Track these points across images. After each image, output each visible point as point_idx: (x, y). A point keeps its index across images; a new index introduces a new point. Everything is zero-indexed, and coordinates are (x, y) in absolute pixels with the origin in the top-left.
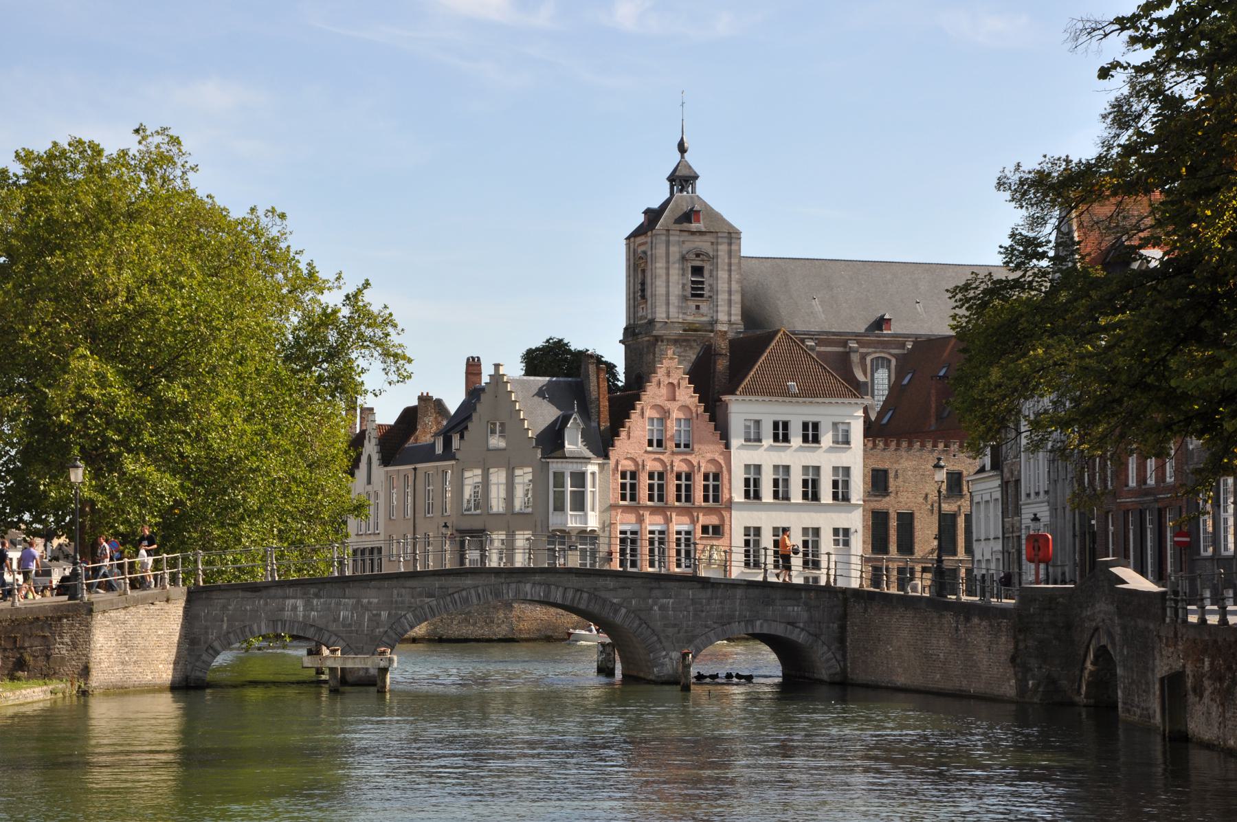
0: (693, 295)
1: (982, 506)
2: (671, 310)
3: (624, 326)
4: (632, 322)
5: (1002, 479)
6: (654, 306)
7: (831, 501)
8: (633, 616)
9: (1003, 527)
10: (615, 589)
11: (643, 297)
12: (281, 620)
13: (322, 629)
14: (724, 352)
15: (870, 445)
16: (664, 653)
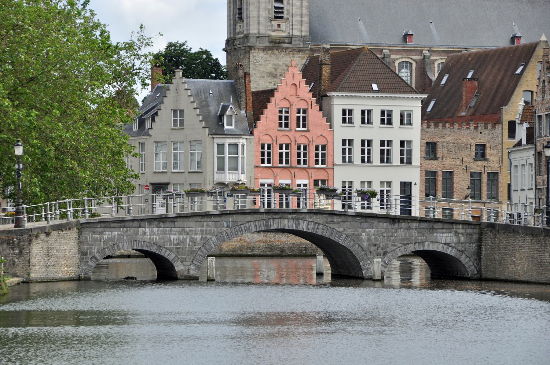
0: (276, 17)
1: (520, 168)
2: (261, 28)
3: (226, 38)
4: (232, 36)
5: (536, 150)
6: (248, 25)
7: (379, 164)
8: (350, 239)
9: (536, 182)
10: (339, 222)
11: (240, 18)
12: (136, 241)
13: (161, 246)
14: (327, 62)
15: (425, 126)
16: (369, 262)
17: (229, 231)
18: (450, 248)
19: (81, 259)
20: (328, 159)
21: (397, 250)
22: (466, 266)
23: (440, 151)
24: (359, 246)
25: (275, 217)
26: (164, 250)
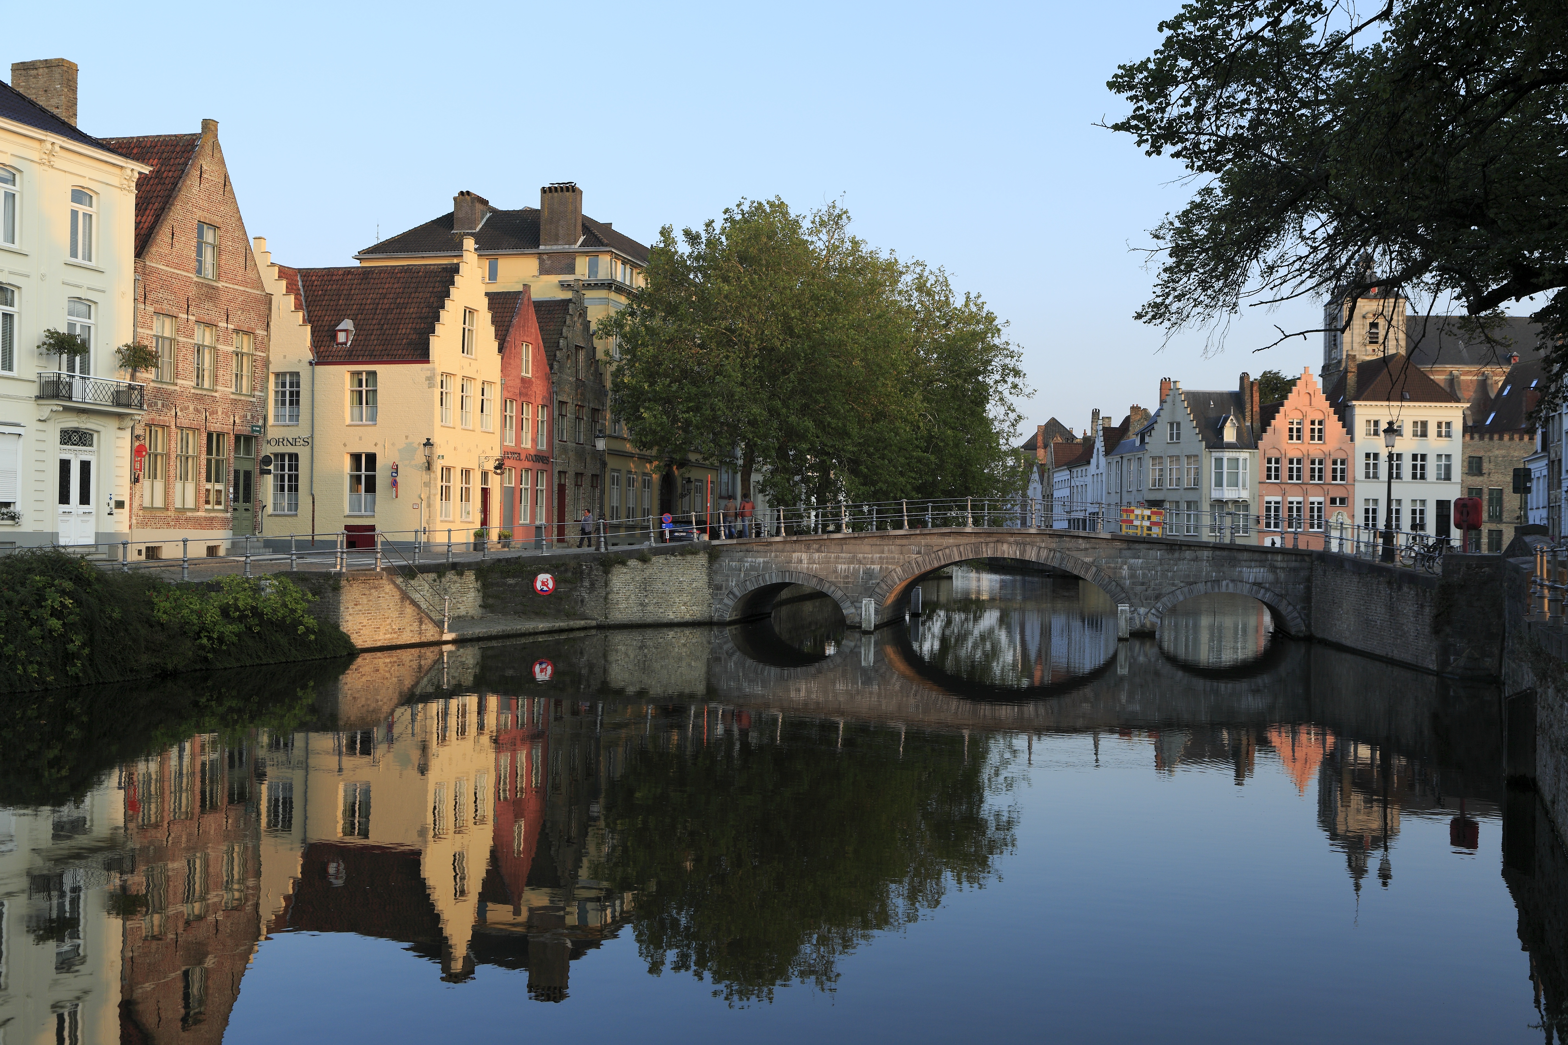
0: (1371, 342)
11: (1335, 345)
15: (1468, 438)
17: (920, 559)
18: (1262, 591)
19: (713, 596)
20: (1349, 475)
21: (1178, 592)
22: (1288, 618)
23: (1486, 466)
24: (1118, 585)
25: (988, 539)
26: (827, 585)
